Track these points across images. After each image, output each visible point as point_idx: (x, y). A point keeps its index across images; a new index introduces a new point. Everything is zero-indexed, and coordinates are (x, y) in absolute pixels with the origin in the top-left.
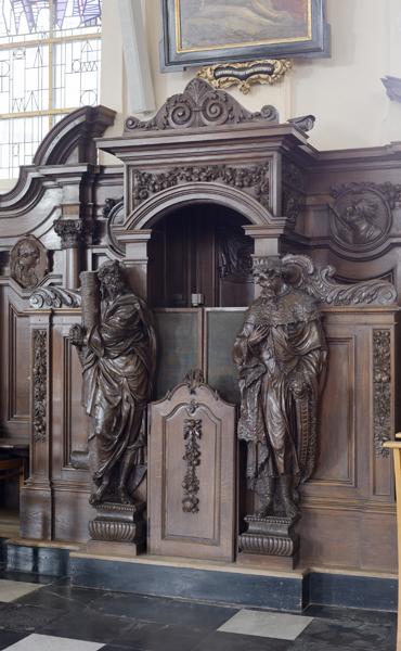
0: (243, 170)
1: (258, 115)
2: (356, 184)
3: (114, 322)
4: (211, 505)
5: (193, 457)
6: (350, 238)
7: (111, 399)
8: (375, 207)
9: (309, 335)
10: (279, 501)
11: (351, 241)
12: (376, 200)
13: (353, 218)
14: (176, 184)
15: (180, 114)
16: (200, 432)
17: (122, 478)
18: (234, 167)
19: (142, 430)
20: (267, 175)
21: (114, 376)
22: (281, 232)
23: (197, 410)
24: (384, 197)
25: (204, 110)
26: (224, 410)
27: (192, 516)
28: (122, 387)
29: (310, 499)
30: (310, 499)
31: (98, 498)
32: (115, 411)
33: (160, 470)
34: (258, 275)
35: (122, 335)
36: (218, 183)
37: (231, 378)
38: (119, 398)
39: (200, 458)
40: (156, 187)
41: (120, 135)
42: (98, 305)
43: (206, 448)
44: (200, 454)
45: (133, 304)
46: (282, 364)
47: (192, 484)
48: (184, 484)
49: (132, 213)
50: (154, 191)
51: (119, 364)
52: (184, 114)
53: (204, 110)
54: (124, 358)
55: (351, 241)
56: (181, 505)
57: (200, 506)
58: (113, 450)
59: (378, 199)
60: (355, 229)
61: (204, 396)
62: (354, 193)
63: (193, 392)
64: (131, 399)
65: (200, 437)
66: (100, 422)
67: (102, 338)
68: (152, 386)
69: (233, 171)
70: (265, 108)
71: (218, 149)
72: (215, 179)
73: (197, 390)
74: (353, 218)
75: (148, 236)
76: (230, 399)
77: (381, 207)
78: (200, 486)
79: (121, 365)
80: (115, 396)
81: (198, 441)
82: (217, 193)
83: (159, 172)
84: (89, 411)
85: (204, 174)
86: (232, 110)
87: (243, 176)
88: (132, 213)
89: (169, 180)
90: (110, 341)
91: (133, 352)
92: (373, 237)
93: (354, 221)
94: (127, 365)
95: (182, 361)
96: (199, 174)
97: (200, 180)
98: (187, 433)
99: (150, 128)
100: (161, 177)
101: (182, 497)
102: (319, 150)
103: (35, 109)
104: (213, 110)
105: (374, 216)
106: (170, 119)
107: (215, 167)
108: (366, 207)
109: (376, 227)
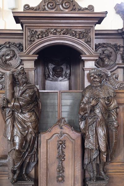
0: (80, 31)
1: (86, 9)
3: (26, 97)
4: (70, 179)
5: (61, 157)
6: (101, 64)
7: (23, 133)
8: (111, 53)
9: (113, 102)
10: (100, 174)
13: (103, 56)
14: (49, 36)
15: (51, 5)
16: (65, 146)
17: (24, 169)
18: (75, 30)
19: (36, 146)
20: (90, 35)
21: (24, 122)
22: (97, 58)
23: (63, 136)
25: (62, 5)
26: (75, 135)
27: (62, 184)
28: (28, 127)
29: (110, 171)
30: (110, 171)
31: (16, 180)
32: (24, 139)
33: (46, 164)
34: (93, 76)
35: (28, 103)
36: (82, 41)
37: (73, 121)
38: (27, 132)
39: (65, 157)
40: (40, 36)
41: (22, 11)
42: (13, 89)
43: (68, 153)
44: (65, 156)
45: (34, 88)
47: (61, 169)
48: (58, 170)
49: (27, 49)
50: (38, 38)
51: (26, 116)
52: (53, 5)
53: (62, 5)
54: (29, 113)
56: (56, 179)
57: (65, 179)
58: (22, 156)
61: (67, 130)
62: (103, 47)
63: (61, 128)
64: (33, 132)
65: (65, 148)
66: (17, 144)
67: (20, 104)
68: (40, 127)
69: (75, 32)
70: (89, 6)
72: (82, 39)
73: (63, 127)
75: (36, 58)
77: (114, 53)
78: (65, 170)
79: (28, 117)
80: (25, 131)
81: (64, 150)
82: (68, 40)
83: (41, 30)
84: (9, 138)
85: (62, 32)
86: (75, 5)
87: (80, 34)
88: (27, 49)
89: (46, 34)
90: (24, 105)
91: (33, 111)
93: (103, 58)
94: (31, 116)
95: (50, 114)
96: (60, 32)
97: (60, 34)
98: (59, 146)
99: (36, 10)
100: (42, 32)
101: (56, 175)
102: (121, 28)
104: (67, 4)
106: (46, 7)
107: (67, 29)
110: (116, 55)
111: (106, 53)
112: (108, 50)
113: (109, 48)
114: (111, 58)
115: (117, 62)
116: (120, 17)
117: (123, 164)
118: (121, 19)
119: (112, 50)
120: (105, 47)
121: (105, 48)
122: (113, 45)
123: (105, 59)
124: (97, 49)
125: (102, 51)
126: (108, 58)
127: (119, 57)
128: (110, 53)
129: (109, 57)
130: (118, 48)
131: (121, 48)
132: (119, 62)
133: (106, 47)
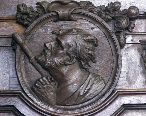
2: (62, 4)
6: (51, 94)
8: (94, 43)
11: (53, 100)
12: (95, 31)
13: (57, 60)
24: (110, 27)
46: (114, 36)
55: (53, 100)
59: (97, 30)
60: (60, 80)
62: (58, 18)
71: (111, 97)
74: (57, 60)
76: (137, 11)
77: (104, 43)
92: (80, 49)
93: (59, 66)
103: (17, 80)
105: (92, 58)
108: (81, 43)
109: (96, 76)
110: (116, 50)
111: (69, 46)
112: (78, 31)
113: (85, 25)
114: (96, 66)
115: (122, 83)
116: (94, 5)
117: (1, 36)
118: (99, 5)
119: (95, 31)
120: (64, 19)
121: (65, 25)
122: (101, 7)
123: (64, 70)
124: (31, 26)
125: (55, 36)
126: (81, 67)
127: (130, 57)
128: (90, 46)
129: (83, 60)
130: (124, 23)
131: (137, 22)
132: (130, 83)
133: (70, 19)
